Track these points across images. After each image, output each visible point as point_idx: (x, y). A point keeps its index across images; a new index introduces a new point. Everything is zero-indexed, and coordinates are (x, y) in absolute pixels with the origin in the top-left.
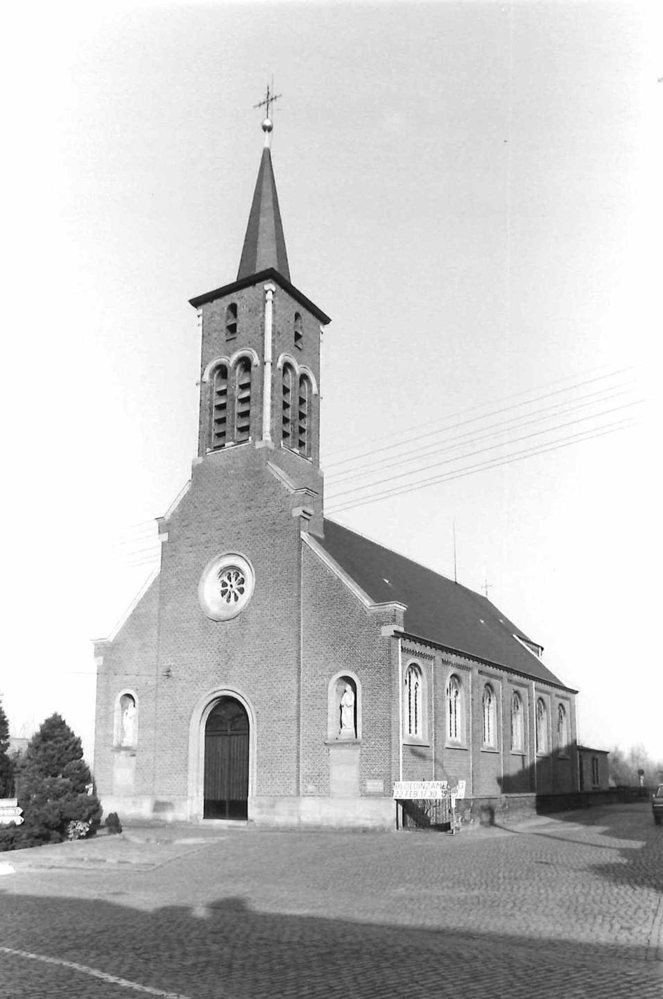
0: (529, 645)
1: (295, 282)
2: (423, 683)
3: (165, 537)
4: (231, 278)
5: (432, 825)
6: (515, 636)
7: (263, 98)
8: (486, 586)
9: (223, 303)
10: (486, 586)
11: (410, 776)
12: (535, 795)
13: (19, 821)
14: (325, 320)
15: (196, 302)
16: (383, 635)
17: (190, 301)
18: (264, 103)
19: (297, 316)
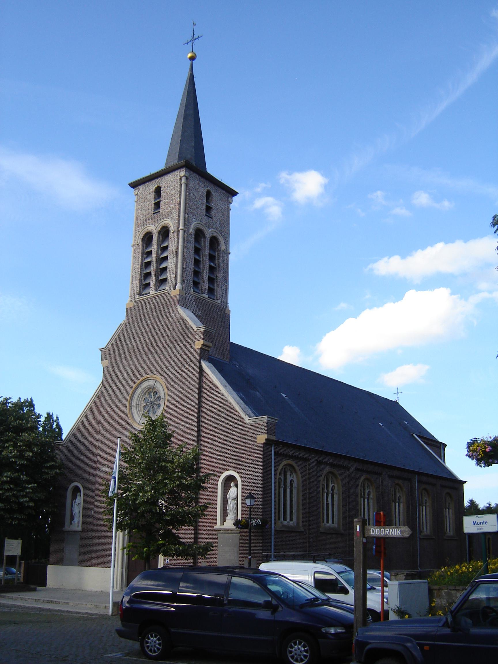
0: (424, 440)
1: (211, 169)
2: (298, 480)
3: (106, 362)
4: (161, 166)
5: (483, 510)
6: (414, 435)
7: (196, 42)
8: (398, 393)
9: (152, 187)
10: (398, 393)
11: (378, 523)
12: (397, 582)
13: (50, 568)
14: (234, 193)
15: (134, 185)
16: (258, 442)
17: (129, 185)
18: (190, 41)
19: (209, 194)
